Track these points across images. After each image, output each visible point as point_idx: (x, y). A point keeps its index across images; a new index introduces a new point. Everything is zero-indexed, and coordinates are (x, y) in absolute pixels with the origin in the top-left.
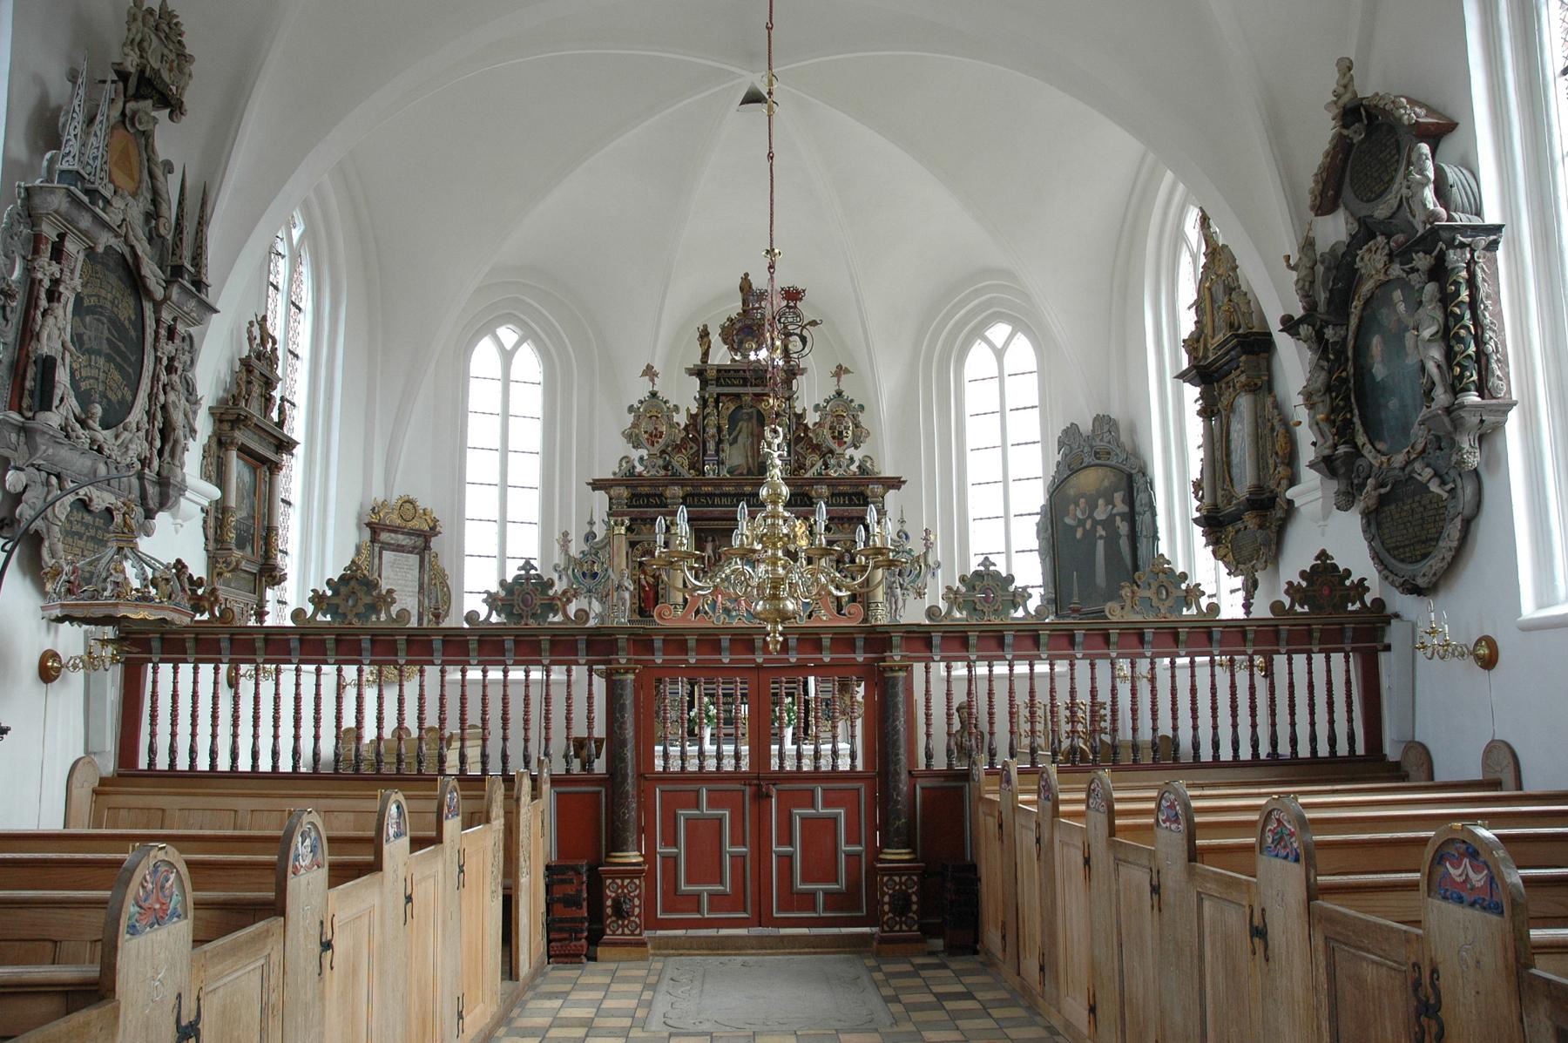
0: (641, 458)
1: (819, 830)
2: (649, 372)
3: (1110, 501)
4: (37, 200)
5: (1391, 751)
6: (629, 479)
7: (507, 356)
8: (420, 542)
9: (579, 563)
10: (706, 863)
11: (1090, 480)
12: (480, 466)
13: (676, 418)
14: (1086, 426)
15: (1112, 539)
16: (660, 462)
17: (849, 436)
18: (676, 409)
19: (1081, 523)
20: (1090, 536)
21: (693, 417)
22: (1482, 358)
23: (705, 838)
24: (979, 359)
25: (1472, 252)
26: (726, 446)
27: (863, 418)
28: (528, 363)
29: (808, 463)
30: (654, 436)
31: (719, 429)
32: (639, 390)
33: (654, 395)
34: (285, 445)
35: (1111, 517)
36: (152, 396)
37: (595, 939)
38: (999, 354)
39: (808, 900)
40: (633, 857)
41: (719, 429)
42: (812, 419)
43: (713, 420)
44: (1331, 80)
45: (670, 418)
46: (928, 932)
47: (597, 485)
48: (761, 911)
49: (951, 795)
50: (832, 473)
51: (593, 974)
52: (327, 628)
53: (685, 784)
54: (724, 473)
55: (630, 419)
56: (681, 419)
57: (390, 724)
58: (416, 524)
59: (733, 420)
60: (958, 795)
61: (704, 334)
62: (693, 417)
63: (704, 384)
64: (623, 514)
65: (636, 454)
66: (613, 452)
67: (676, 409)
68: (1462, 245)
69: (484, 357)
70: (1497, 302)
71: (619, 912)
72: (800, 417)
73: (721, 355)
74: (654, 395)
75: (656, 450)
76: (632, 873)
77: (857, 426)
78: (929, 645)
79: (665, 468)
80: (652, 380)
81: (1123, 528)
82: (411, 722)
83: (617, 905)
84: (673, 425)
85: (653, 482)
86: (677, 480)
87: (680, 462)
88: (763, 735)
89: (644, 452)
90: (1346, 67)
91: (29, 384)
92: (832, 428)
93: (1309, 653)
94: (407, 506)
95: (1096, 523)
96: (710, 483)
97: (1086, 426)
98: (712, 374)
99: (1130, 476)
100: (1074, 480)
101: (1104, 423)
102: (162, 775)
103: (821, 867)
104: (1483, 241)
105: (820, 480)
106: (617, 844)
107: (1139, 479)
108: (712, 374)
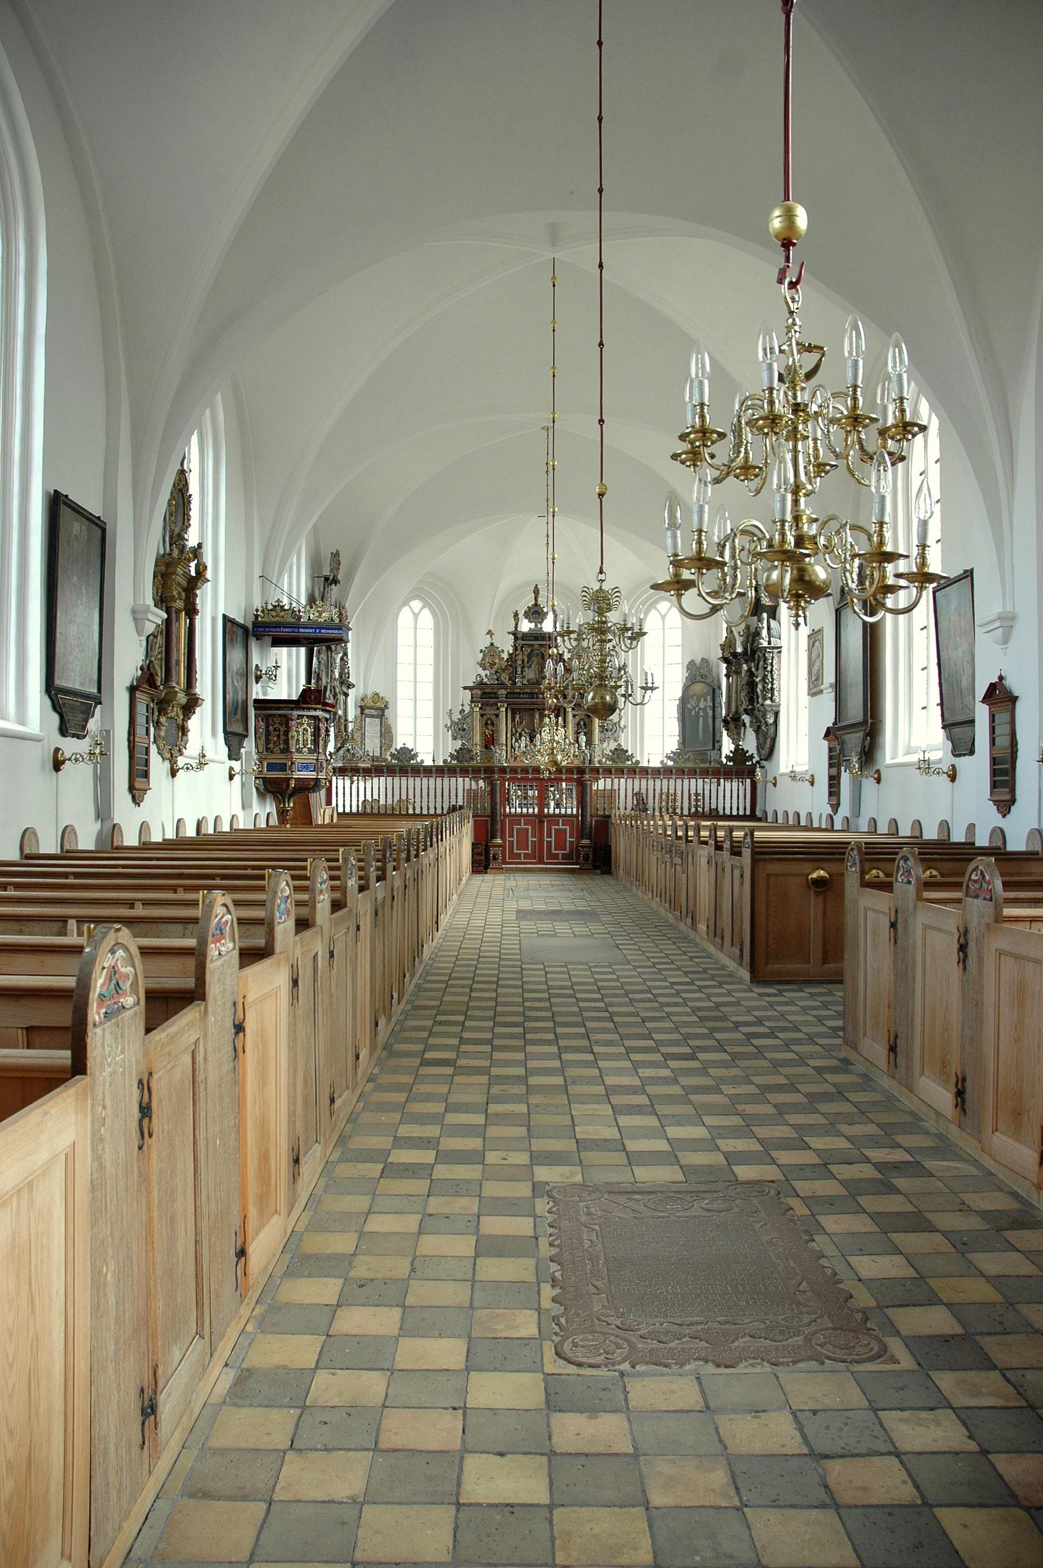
1: (560, 833)
2: (490, 632)
3: (705, 700)
5: (758, 814)
6: (480, 685)
7: (416, 616)
8: (380, 712)
9: (457, 724)
10: (523, 844)
11: (698, 688)
12: (404, 672)
13: (503, 655)
14: (698, 661)
15: (705, 717)
18: (503, 651)
19: (694, 708)
20: (697, 714)
21: (510, 655)
23: (523, 835)
26: (526, 669)
28: (427, 619)
30: (492, 665)
31: (523, 661)
32: (484, 642)
33: (492, 644)
35: (706, 707)
37: (486, 867)
38: (663, 617)
39: (556, 856)
40: (499, 841)
41: (523, 661)
43: (520, 657)
46: (595, 868)
47: (465, 688)
48: (539, 858)
49: (604, 822)
51: (488, 877)
52: (394, 766)
53: (516, 818)
54: (525, 682)
56: (505, 656)
57: (397, 798)
58: (379, 705)
59: (529, 656)
60: (607, 822)
61: (516, 615)
62: (510, 655)
63: (516, 639)
65: (483, 673)
66: (473, 672)
67: (503, 651)
69: (405, 616)
70: (779, 670)
71: (495, 858)
72: (561, 655)
73: (526, 626)
75: (493, 671)
76: (499, 846)
78: (598, 773)
81: (710, 713)
82: (369, 798)
83: (494, 856)
86: (502, 685)
87: (505, 677)
88: (542, 802)
89: (487, 672)
93: (683, 779)
95: (700, 709)
96: (519, 688)
97: (698, 661)
98: (520, 636)
99: (714, 690)
100: (692, 687)
101: (704, 661)
102: (354, 814)
103: (560, 846)
104: (776, 651)
106: (494, 837)
108: (520, 636)
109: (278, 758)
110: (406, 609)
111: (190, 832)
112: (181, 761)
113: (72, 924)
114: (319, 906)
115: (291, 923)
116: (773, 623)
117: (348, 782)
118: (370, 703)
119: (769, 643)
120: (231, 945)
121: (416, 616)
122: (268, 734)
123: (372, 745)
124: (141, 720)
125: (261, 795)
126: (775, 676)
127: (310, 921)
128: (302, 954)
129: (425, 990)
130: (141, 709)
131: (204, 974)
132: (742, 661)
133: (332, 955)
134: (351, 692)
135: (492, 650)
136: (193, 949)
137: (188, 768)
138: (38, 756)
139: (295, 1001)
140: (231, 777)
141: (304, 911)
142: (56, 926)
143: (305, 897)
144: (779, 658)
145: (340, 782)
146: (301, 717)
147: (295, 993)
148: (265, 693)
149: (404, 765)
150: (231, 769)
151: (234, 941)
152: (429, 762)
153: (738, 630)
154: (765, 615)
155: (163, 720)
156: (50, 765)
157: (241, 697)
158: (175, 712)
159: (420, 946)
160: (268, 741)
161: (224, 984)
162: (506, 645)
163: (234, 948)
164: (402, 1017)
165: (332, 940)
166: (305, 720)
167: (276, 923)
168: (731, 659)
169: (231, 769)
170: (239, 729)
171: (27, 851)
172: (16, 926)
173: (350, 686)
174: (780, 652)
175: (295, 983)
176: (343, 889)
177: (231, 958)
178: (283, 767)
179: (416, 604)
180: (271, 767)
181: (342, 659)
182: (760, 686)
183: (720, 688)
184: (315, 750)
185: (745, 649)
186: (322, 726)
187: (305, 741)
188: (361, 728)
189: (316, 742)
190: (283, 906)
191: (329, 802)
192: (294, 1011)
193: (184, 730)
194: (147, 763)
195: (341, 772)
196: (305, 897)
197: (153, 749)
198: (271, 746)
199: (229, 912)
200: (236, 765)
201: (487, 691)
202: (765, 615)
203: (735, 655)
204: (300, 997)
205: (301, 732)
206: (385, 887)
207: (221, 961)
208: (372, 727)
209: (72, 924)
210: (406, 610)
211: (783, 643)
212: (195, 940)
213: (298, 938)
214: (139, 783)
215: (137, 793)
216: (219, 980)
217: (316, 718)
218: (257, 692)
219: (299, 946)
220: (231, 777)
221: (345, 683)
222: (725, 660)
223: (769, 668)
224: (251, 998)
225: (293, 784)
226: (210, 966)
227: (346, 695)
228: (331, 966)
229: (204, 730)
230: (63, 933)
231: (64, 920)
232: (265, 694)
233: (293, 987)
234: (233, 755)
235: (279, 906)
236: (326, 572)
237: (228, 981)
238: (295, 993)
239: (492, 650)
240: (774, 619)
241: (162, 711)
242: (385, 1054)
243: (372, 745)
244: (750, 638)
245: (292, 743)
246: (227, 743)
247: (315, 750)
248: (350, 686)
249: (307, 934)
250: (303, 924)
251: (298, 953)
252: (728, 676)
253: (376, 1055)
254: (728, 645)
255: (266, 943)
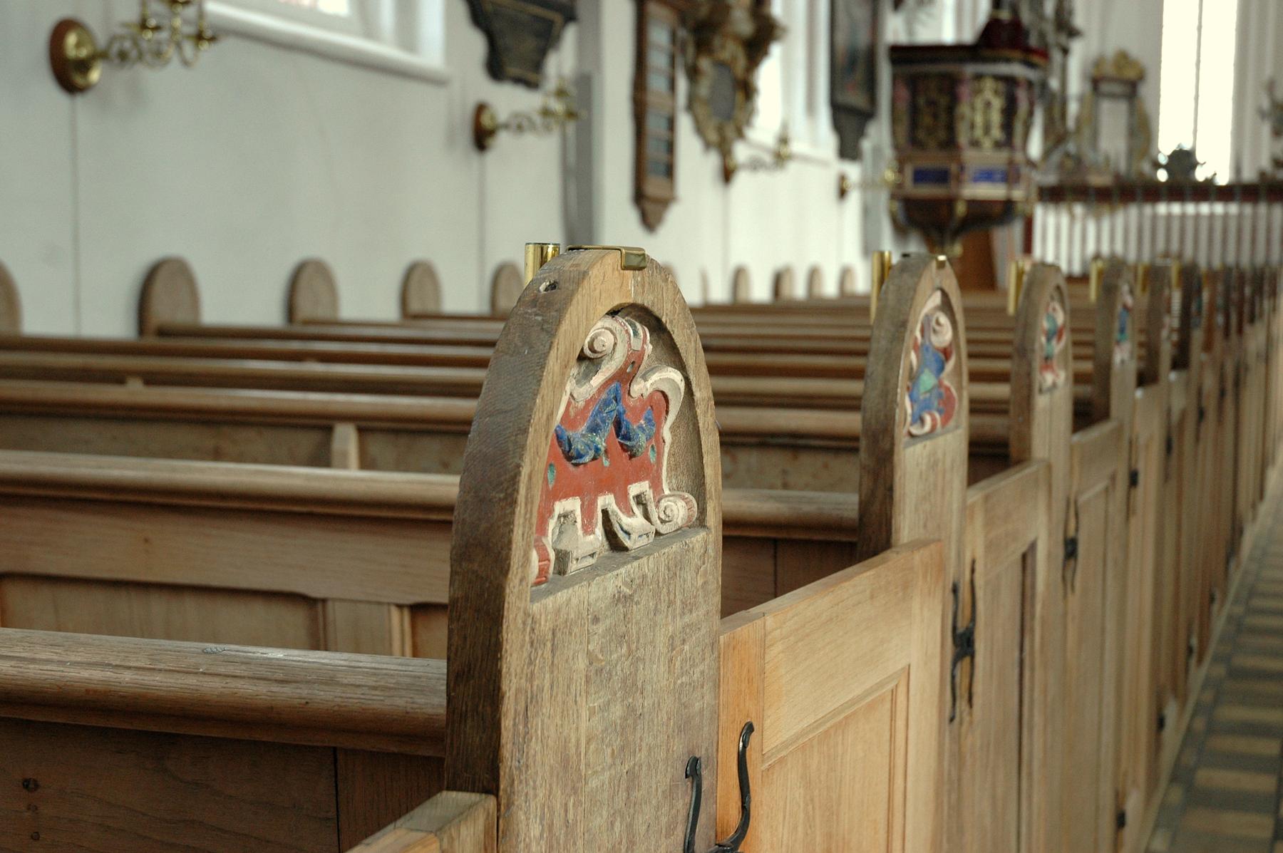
57: (1161, 245)
109: (932, 159)
111: (760, 292)
112: (741, 152)
113: (346, 439)
114: (1041, 402)
115: (952, 444)
117: (1065, 220)
118: (1109, 70)
120: (678, 509)
122: (914, 111)
123: (1112, 143)
124: (658, 60)
125: (900, 231)
127: (1014, 451)
128: (990, 546)
129: (1253, 631)
130: (659, 36)
131: (493, 650)
133: (1071, 548)
134: (1077, 47)
136: (449, 508)
137: (755, 165)
138: (436, 117)
139: (962, 704)
140: (842, 193)
141: (995, 425)
142: (306, 441)
143: (1000, 391)
145: (1051, 220)
146: (979, 77)
147: (962, 681)
148: (910, 31)
149: (1183, 181)
150: (842, 178)
151: (698, 490)
152: (1223, 180)
155: (705, 64)
156: (466, 136)
157: (863, 39)
158: (731, 51)
159: (1237, 531)
160: (914, 125)
161: (631, 686)
163: (701, 522)
164: (1208, 696)
165: (1073, 508)
166: (989, 85)
167: (901, 434)
169: (842, 178)
170: (856, 99)
171: (415, 306)
172: (204, 437)
173: (1073, 33)
175: (963, 644)
176: (1103, 373)
177: (676, 567)
178: (942, 177)
180: (920, 176)
184: (1007, 142)
186: (1022, 95)
187: (987, 129)
188: (1090, 119)
189: (1008, 126)
190: (928, 380)
191: (1028, 248)
192: (957, 740)
193: (747, 90)
194: (671, 147)
195: (1053, 195)
196: (1000, 391)
197: (685, 124)
198: (921, 135)
199: (673, 356)
200: (853, 171)
204: (978, 688)
205: (980, 109)
206: (1187, 383)
207: (613, 582)
208: (1113, 118)
209: (346, 439)
212: (456, 479)
213: (976, 495)
214: (654, 187)
215: (650, 203)
216: (598, 673)
217: (1010, 81)
218: (895, 29)
219: (979, 520)
220: (842, 193)
221: (1065, 27)
224: (781, 727)
225: (961, 209)
226: (527, 608)
227: (1065, 51)
228: (1067, 581)
229: (787, 90)
230: (322, 458)
231: (323, 424)
232: (910, 31)
233: (957, 659)
234: (848, 151)
235: (913, 377)
237: (656, 674)
238: (962, 681)
241: (703, 46)
242: (1176, 795)
243: (1112, 143)
245: (963, 139)
246: (837, 125)
247: (1007, 142)
248: (1073, 33)
249: (1006, 484)
250: (991, 455)
251: (976, 545)
253: (1157, 800)
255: (864, 507)
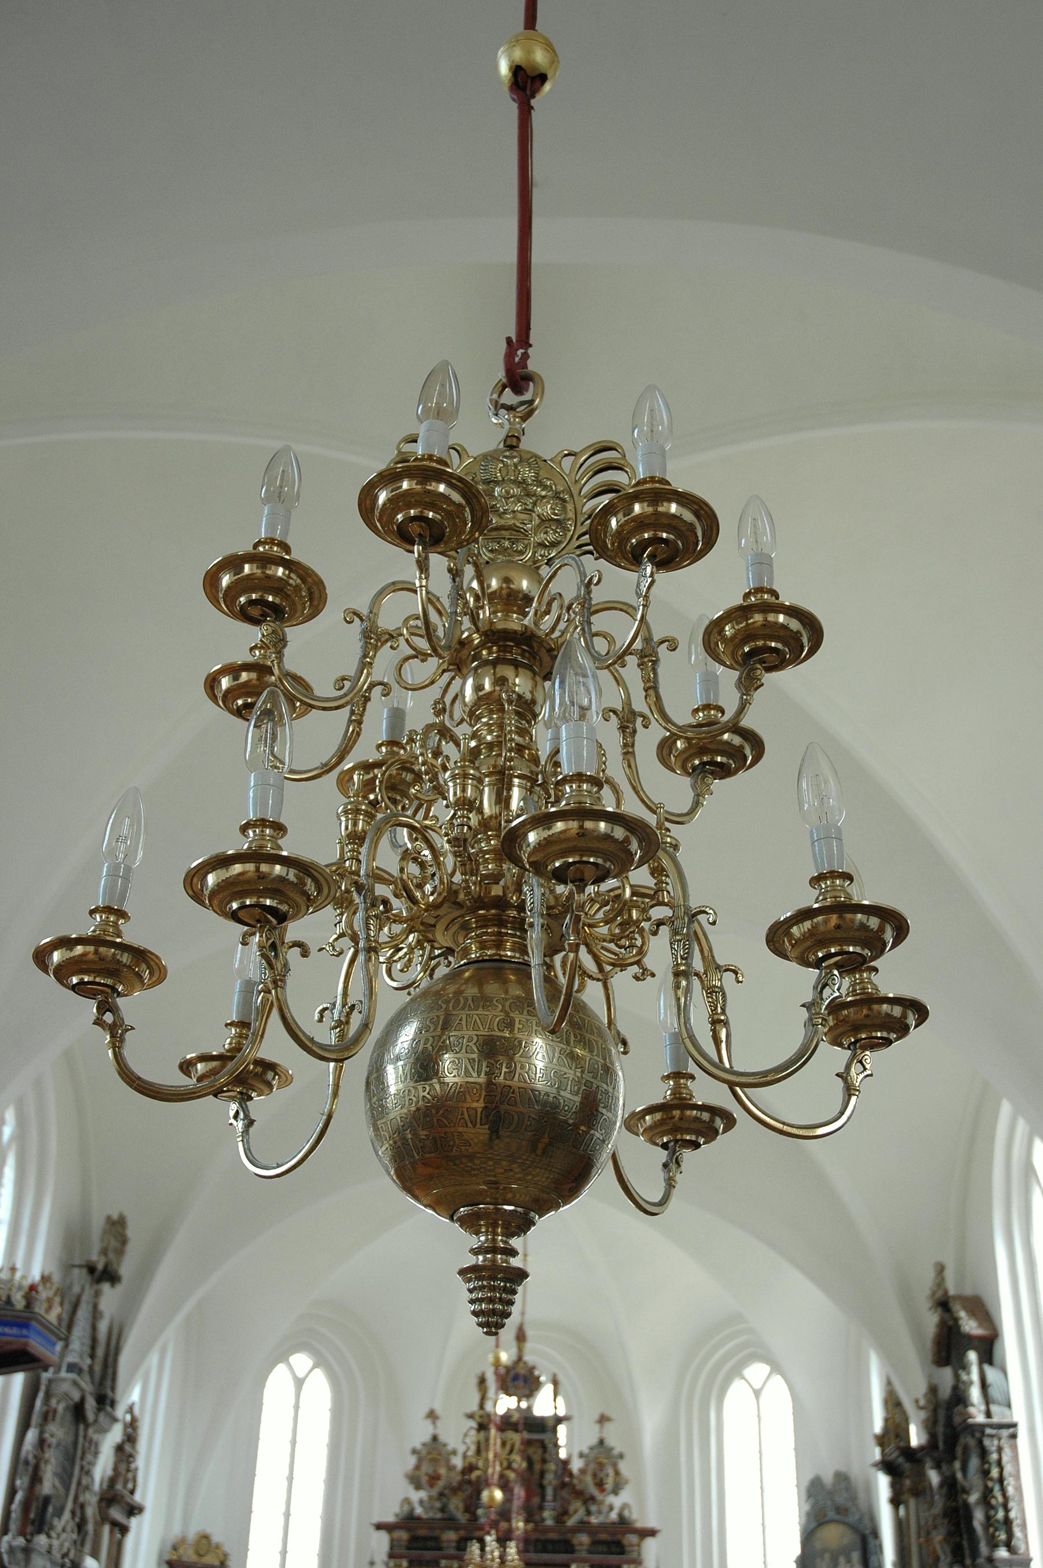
0: (421, 1502)
2: (432, 1415)
4: (53, 1386)
6: (408, 1521)
7: (299, 1383)
14: (828, 1478)
16: (438, 1505)
17: (609, 1485)
22: (1008, 1522)
24: (737, 1394)
25: (1000, 1439)
27: (623, 1466)
28: (319, 1390)
29: (572, 1508)
30: (434, 1479)
32: (421, 1434)
33: (435, 1438)
34: (134, 1510)
36: (76, 1497)
42: (576, 1465)
44: (929, 1277)
45: (448, 1461)
47: (379, 1527)
50: (594, 1520)
55: (412, 1461)
56: (458, 1462)
61: (482, 1381)
64: (401, 1557)
66: (396, 1495)
68: (992, 1436)
69: (278, 1383)
70: (1017, 1477)
72: (565, 1463)
73: (505, 1404)
74: (435, 1438)
75: (434, 1492)
77: (617, 1473)
79: (443, 1510)
80: (434, 1423)
84: (451, 1468)
85: (429, 1523)
86: (450, 1522)
90: (940, 1269)
91: (32, 1515)
92: (595, 1475)
94: (204, 1541)
97: (828, 1478)
101: (842, 1478)
104: (1005, 1433)
105: (583, 1526)
107: (872, 1542)
110: (281, 1369)
116: (991, 1374)
119: (988, 1414)
121: (299, 1383)
126: (1010, 1491)
132: (928, 1464)
135: (433, 1451)
144: (1014, 1448)
153: (913, 1392)
154: (972, 1356)
162: (458, 1438)
168: (901, 1463)
174: (1014, 1436)
179: (301, 1361)
181: (119, 1449)
182: (979, 1516)
183: (876, 1534)
185: (932, 1436)
201: (422, 1532)
202: (972, 1356)
203: (909, 1453)
210: (280, 1370)
211: (1018, 1414)
222: (888, 1466)
223: (995, 1473)
236: (95, 1256)
239: (433, 1451)
240: (991, 1363)
244: (942, 1413)
248: (134, 1510)
252: (895, 1501)
254: (894, 1431)
